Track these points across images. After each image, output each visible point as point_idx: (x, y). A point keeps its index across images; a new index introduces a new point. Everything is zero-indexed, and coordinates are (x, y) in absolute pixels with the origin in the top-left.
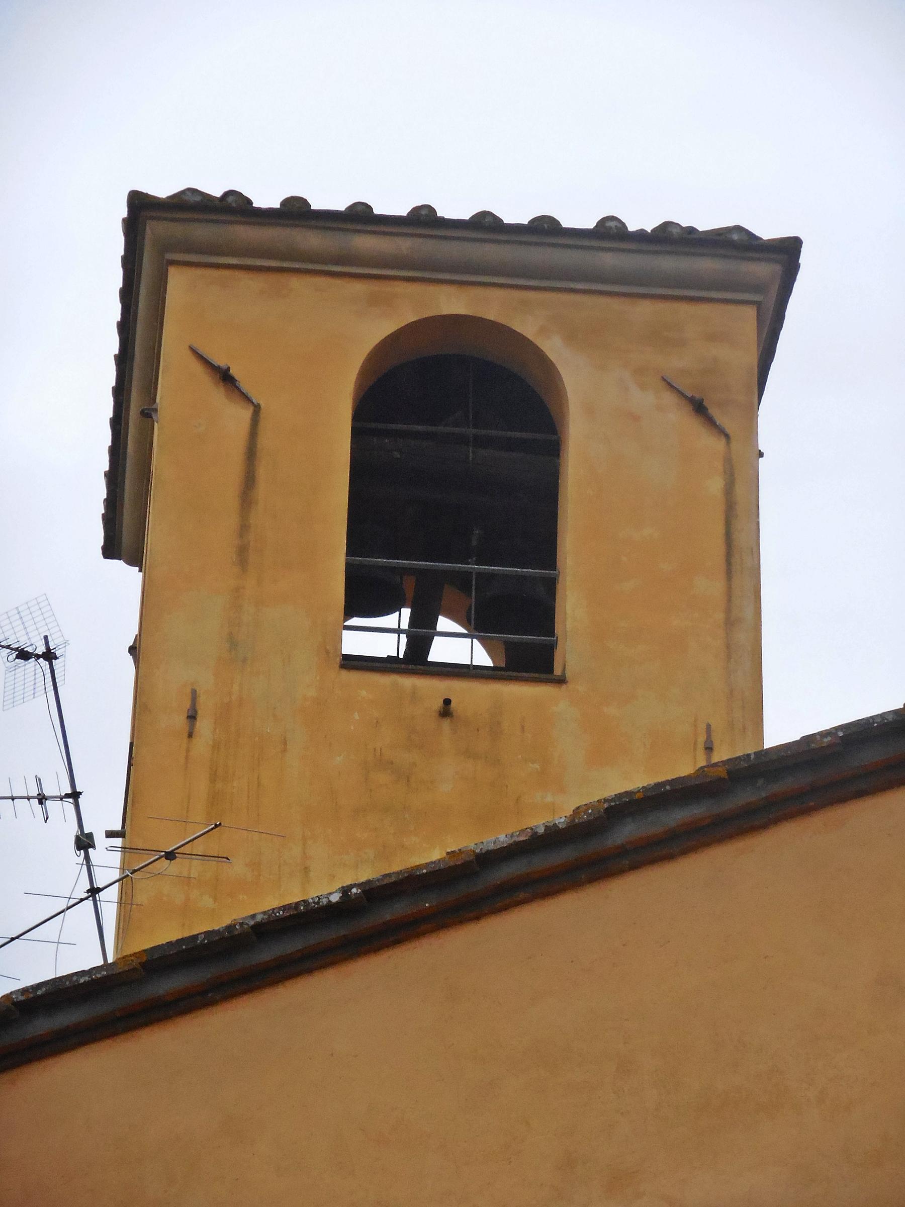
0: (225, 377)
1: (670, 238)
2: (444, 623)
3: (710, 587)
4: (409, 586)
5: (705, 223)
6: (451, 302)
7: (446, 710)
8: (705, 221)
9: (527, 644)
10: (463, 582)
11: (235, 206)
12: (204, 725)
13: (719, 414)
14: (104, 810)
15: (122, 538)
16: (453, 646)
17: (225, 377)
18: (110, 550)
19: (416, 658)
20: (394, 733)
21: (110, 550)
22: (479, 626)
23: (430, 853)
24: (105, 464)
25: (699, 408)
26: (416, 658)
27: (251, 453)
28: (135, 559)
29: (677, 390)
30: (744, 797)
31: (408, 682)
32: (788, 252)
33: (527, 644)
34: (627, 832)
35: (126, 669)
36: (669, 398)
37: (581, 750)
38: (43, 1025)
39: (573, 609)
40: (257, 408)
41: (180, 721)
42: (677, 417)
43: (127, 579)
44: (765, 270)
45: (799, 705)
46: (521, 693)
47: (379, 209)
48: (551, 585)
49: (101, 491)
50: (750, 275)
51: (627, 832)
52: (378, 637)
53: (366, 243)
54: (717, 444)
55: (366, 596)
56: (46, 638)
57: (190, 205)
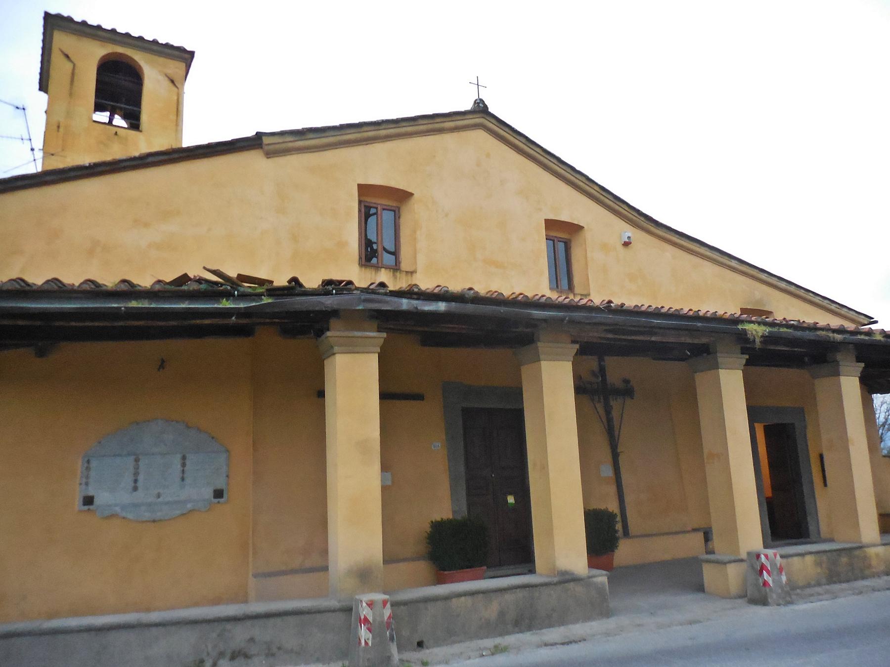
0: (67, 56)
1: (167, 46)
2: (116, 116)
3: (173, 117)
4: (109, 108)
5: (176, 45)
6: (120, 50)
7: (116, 133)
8: (176, 44)
9: (134, 122)
10: (121, 109)
11: (69, 19)
12: (61, 129)
13: (176, 83)
14: (38, 143)
15: (43, 86)
16: (118, 121)
17: (67, 56)
18: (41, 89)
19: (110, 122)
20: (99, 133)
21: (41, 89)
22: (125, 117)
23: (109, 158)
24: (39, 71)
25: (172, 82)
26: (110, 122)
27: (73, 74)
28: (46, 92)
29: (315, 612)
30: (176, 156)
31: (108, 127)
32: (192, 54)
33: (134, 122)
34: (150, 159)
35: (44, 116)
36: (166, 79)
37: (143, 143)
38: (19, 183)
39: (145, 117)
40: (74, 65)
41: (56, 127)
42: (167, 83)
43: (44, 97)
44: (187, 56)
45: (189, 140)
46: (133, 133)
47: (104, 27)
48: (140, 112)
49: (38, 77)
50: (185, 57)
51: (150, 159)
52: (103, 117)
53: (100, 33)
54: (175, 89)
55: (99, 108)
56: (204, 268)
57: (59, 17)
